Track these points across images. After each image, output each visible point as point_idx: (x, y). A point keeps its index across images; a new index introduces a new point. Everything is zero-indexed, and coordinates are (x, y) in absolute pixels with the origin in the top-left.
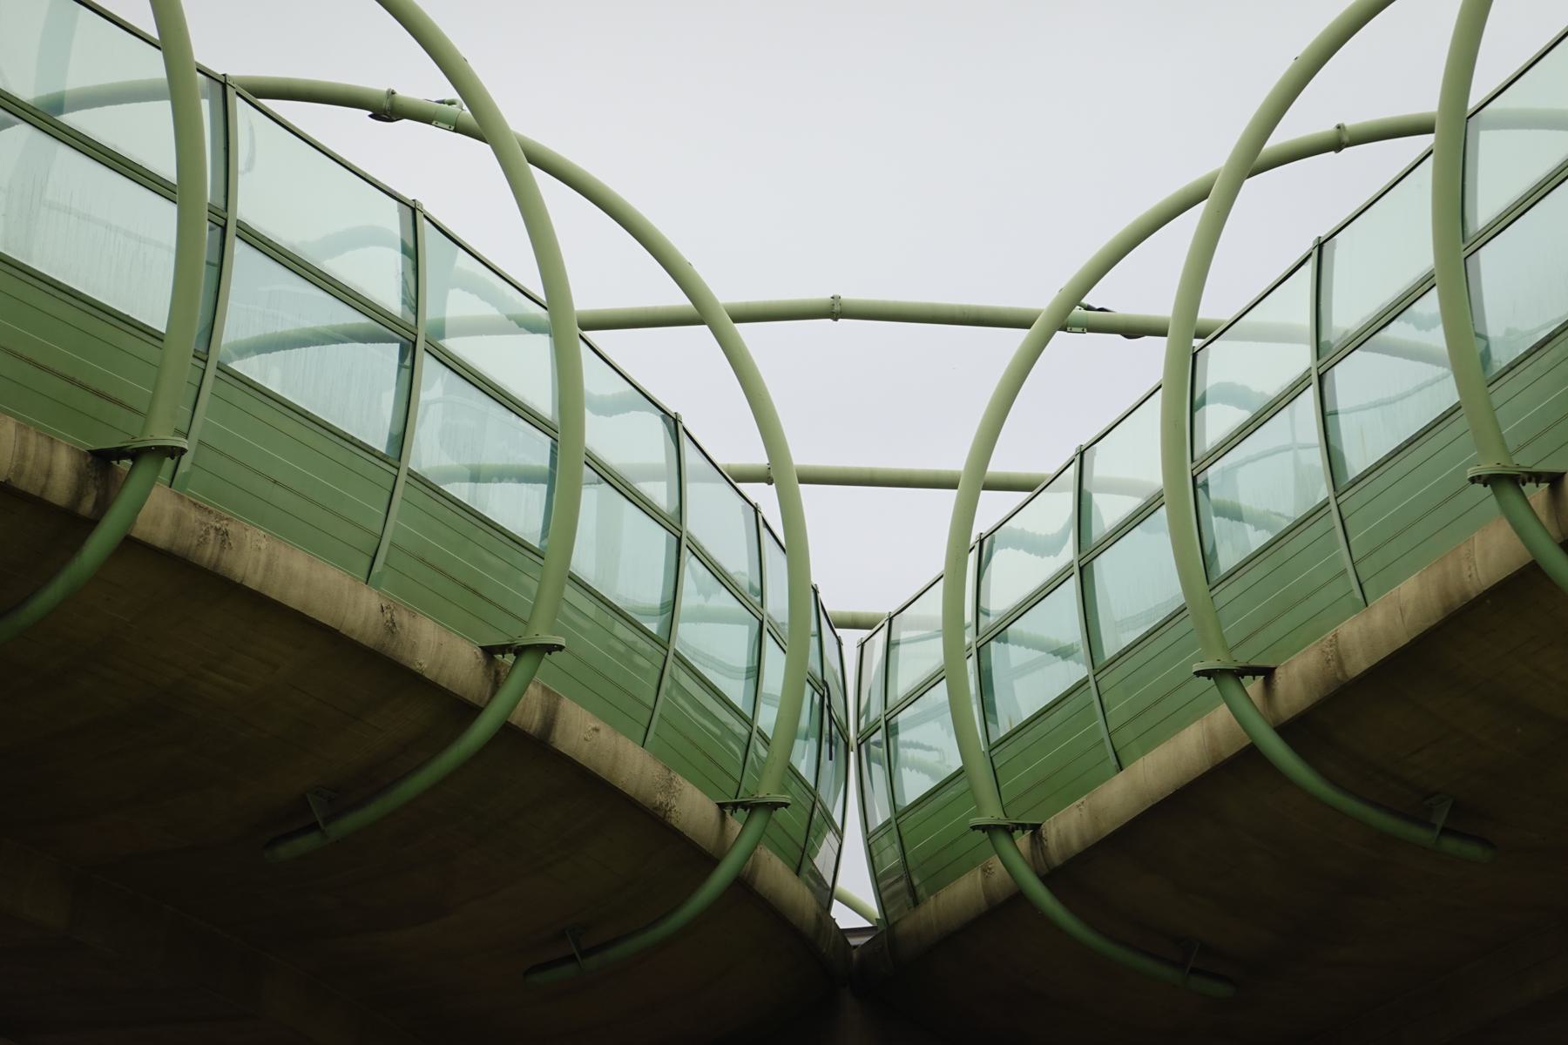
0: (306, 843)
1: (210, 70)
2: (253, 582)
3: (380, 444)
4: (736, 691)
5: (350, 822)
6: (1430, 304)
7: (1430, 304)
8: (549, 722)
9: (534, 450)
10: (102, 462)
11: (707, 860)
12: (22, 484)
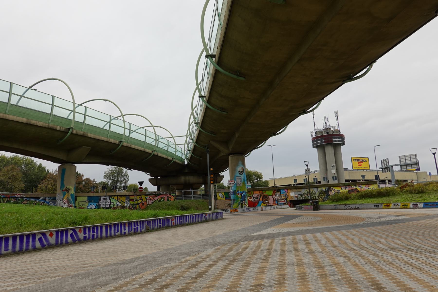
0: (144, 161)
1: (85, 120)
2: (133, 148)
3: (167, 150)
4: (229, 170)
5: (146, 159)
6: (76, 106)
7: (76, 106)
8: (158, 154)
9: (175, 150)
10: (121, 142)
11: (172, 161)
12: (114, 143)
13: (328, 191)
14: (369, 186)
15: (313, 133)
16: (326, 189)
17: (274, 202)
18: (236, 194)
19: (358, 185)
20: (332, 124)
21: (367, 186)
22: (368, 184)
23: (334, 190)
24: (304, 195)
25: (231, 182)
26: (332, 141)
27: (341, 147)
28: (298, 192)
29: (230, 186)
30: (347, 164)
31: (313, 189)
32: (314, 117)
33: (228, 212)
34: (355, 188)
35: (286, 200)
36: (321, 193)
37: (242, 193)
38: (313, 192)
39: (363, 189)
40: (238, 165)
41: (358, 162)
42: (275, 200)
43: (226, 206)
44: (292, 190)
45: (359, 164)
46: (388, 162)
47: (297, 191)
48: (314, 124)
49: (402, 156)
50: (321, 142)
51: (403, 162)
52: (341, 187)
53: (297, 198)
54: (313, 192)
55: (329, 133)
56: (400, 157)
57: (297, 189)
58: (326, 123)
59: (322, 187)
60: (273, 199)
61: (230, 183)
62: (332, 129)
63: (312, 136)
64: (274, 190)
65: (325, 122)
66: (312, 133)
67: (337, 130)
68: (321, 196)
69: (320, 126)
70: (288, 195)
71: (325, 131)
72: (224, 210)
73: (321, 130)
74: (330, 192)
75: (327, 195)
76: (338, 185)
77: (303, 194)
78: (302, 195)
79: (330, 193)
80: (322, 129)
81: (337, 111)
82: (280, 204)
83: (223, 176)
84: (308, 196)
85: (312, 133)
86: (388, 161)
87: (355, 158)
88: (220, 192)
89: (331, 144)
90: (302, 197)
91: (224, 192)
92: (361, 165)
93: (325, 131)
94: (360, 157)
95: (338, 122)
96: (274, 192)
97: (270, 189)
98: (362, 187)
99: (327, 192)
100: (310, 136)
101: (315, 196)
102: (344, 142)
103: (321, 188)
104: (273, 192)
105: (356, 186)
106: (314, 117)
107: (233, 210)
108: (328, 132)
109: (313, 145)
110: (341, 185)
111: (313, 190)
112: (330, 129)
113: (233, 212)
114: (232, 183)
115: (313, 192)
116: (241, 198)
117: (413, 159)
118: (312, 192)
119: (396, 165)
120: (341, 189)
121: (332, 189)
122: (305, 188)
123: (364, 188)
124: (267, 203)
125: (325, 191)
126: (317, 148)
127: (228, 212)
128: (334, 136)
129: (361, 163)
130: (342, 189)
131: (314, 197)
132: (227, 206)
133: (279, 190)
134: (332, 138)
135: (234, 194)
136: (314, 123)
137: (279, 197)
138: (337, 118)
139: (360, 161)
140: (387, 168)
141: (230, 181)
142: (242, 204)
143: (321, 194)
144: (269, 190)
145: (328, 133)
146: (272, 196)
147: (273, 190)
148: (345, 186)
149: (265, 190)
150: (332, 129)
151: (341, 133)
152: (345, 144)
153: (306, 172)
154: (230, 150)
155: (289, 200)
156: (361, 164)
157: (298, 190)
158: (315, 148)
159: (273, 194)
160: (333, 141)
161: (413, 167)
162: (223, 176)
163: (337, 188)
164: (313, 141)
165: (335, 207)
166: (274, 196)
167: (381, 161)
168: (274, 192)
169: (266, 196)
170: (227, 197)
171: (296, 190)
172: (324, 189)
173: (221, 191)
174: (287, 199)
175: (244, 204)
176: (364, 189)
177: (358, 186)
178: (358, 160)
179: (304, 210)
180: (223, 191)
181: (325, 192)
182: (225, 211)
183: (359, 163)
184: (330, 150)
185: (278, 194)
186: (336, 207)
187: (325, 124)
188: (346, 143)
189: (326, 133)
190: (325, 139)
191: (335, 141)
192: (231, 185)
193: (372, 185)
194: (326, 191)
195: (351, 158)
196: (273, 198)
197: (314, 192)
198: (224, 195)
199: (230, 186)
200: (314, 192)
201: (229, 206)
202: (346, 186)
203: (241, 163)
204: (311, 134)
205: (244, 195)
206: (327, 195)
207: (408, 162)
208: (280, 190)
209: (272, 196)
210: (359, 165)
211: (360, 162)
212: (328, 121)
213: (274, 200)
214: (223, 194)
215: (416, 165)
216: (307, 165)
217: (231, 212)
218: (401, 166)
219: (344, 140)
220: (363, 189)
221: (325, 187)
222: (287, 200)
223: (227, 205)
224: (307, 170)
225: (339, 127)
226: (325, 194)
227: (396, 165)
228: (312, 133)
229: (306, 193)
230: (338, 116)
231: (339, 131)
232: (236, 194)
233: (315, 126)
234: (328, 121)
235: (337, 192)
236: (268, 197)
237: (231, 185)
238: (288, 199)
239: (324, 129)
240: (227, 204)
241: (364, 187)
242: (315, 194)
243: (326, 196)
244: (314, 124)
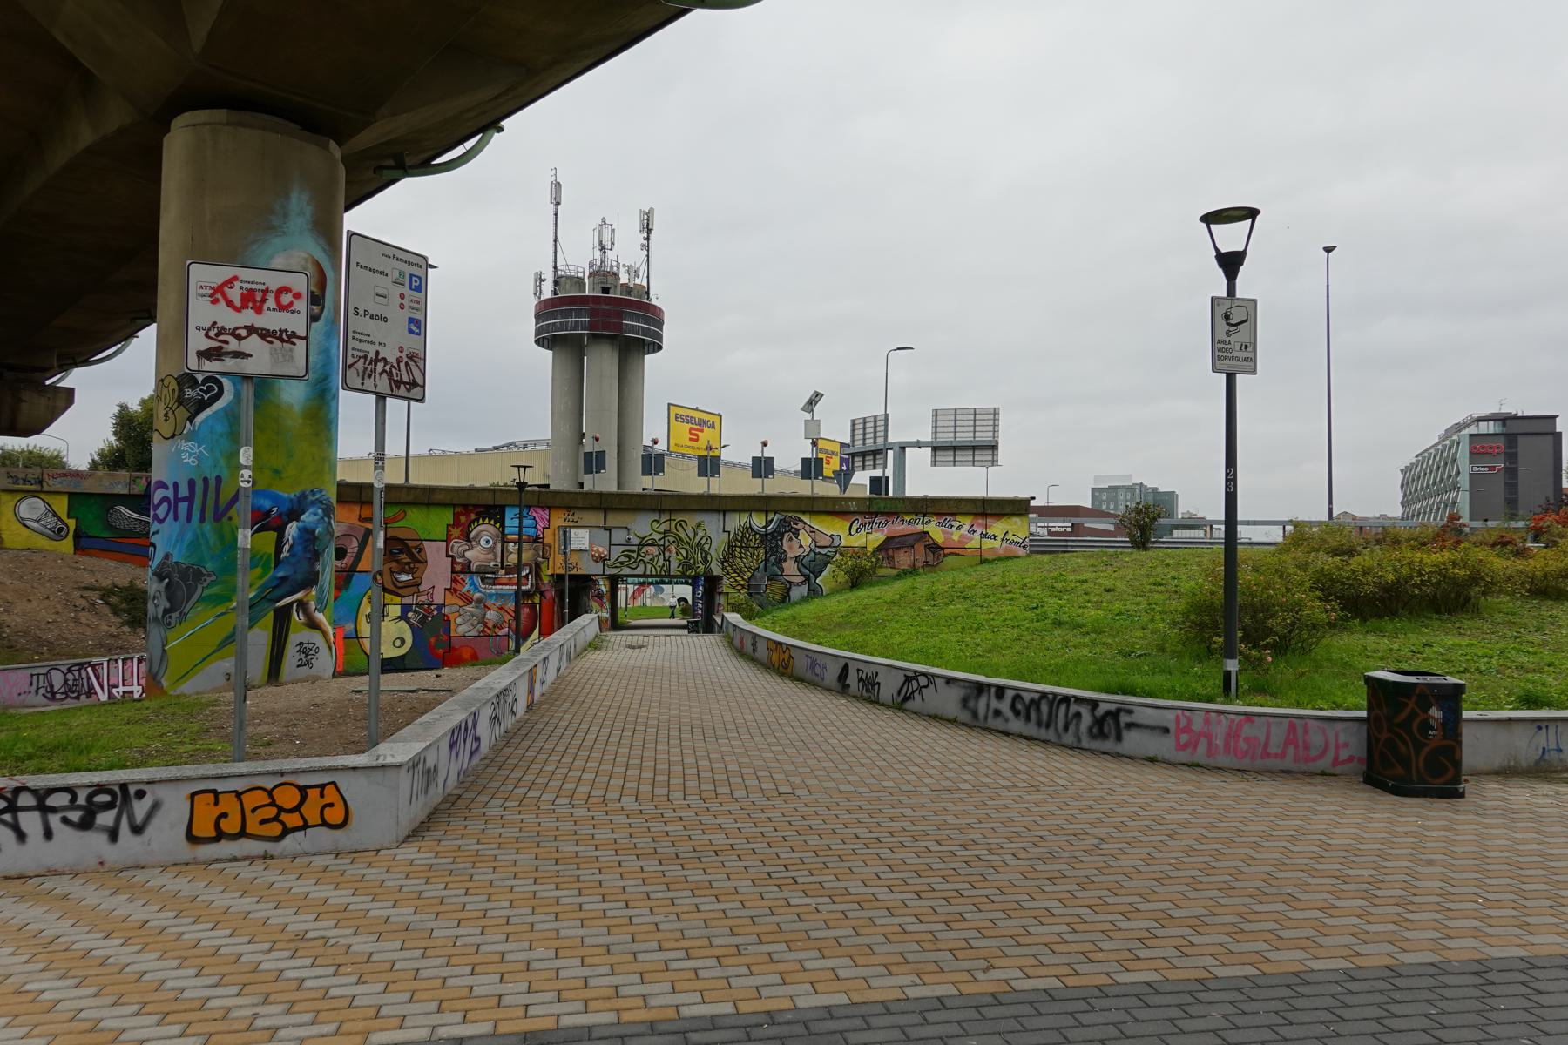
13: (777, 536)
14: (989, 521)
15: (544, 280)
16: (768, 523)
17: (454, 581)
18: (218, 517)
19: (938, 514)
20: (626, 255)
21: (980, 521)
22: (989, 512)
23: (813, 531)
24: (644, 550)
25: (248, 317)
26: (619, 327)
27: (646, 357)
28: (609, 530)
29: (211, 366)
30: (654, 429)
31: (698, 518)
32: (556, 215)
33: (137, 830)
34: (920, 527)
35: (530, 572)
36: (739, 543)
37: (294, 514)
38: (698, 538)
39: (956, 538)
40: (271, 229)
41: (690, 425)
42: (462, 569)
43: (83, 603)
44: (578, 514)
45: (691, 434)
46: (886, 431)
47: (608, 525)
48: (555, 245)
49: (965, 412)
50: (576, 325)
51: (946, 437)
52: (848, 516)
53: (601, 564)
54: (696, 534)
55: (611, 291)
56: (936, 413)
57: (606, 510)
58: (603, 249)
59: (750, 511)
60: (454, 562)
61: (229, 319)
62: (624, 279)
63: (538, 292)
64: (465, 506)
65: (601, 242)
66: (542, 280)
67: (641, 286)
68: (741, 558)
69: (579, 259)
70: (550, 546)
71: (597, 279)
72: (44, 809)
73: (580, 275)
74: (791, 539)
75: (772, 558)
76: (837, 508)
77: (640, 546)
78: (635, 548)
79: (791, 548)
80: (584, 272)
81: (651, 210)
82: (491, 595)
83: (70, 393)
84: (667, 554)
85: (540, 280)
86: (886, 425)
87: (681, 411)
88: (32, 494)
89: (612, 338)
90: (630, 557)
91: (71, 495)
92: (697, 440)
93: (597, 279)
94: (697, 409)
95: (648, 256)
96: (463, 519)
97: (438, 497)
98: (956, 524)
99: (772, 541)
100: (532, 292)
101: (705, 561)
102: (660, 337)
103: (747, 515)
104: (456, 516)
105: (926, 519)
106: (556, 215)
107: (250, 801)
108: (609, 286)
109: (538, 331)
110: (853, 507)
111: (699, 525)
112: (616, 275)
113: (242, 834)
114: (265, 335)
115: (698, 538)
116: (278, 562)
117: (963, 429)
118: (691, 535)
119: (919, 444)
120: (848, 528)
121: (800, 526)
122: (653, 510)
123: (964, 530)
124: (407, 585)
125: (764, 536)
126: (549, 348)
127: (137, 830)
128: (630, 307)
129: (699, 433)
130: (853, 531)
131: (702, 567)
132: (93, 604)
133: (495, 507)
134: (620, 315)
135: (196, 515)
136: (555, 241)
137: (492, 549)
138: (648, 239)
139: (697, 422)
140: (875, 453)
141: (235, 294)
142: (282, 617)
143: (741, 547)
144: (429, 505)
145: (605, 290)
146: (445, 543)
147: (454, 506)
148: (870, 513)
149: (402, 504)
150: (624, 279)
151: (654, 302)
152: (660, 348)
153: (1221, 335)
154: (199, 33)
155: (552, 575)
156: (697, 435)
157: (614, 519)
158: (543, 346)
159: (456, 532)
160: (624, 327)
161: (957, 458)
162: (70, 393)
163: (828, 519)
164: (539, 317)
165: (1541, 739)
166: (458, 546)
167: (853, 423)
168: (463, 519)
169: (402, 541)
170: (97, 530)
171: (601, 515)
172: (758, 521)
173: (40, 482)
174: (538, 566)
175: (297, 618)
176: (962, 536)
177: (935, 520)
178: (690, 420)
179: (1184, 756)
180: (59, 487)
181: (761, 542)
182: (86, 824)
183: (691, 429)
184: (601, 363)
185: (485, 531)
186: (1553, 746)
187: (598, 254)
188: (664, 345)
189: (598, 288)
190: (592, 313)
191: (632, 329)
192: (230, 364)
193: (1004, 520)
194: (766, 535)
195: (669, 409)
196: (448, 556)
197: (701, 533)
198: (64, 518)
199: (211, 366)
200: (701, 533)
201: (106, 610)
202: (877, 514)
203: (308, 210)
204: (536, 281)
205: (307, 535)
206: (772, 558)
207: (965, 436)
208: (502, 509)
209: (448, 540)
210: (691, 439)
211: (695, 426)
212: (613, 243)
213: (453, 571)
214: (61, 505)
215: (990, 452)
216: (1231, 263)
217: (204, 828)
218: (935, 449)
219: (662, 330)
220: (956, 538)
221: (767, 513)
222: (538, 576)
223: (94, 596)
224: (1227, 317)
225: (648, 277)
226: (762, 551)
227: (919, 444)
228: (542, 280)
229: (657, 537)
230: (649, 231)
231: (648, 293)
232: (218, 517)
233: (555, 252)
234: (613, 243)
235: (827, 542)
236: (421, 550)
237: (248, 367)
238: (544, 566)
239: (591, 274)
240: (93, 589)
241: (966, 527)
242: (706, 547)
243: (766, 560)
244: (555, 245)
